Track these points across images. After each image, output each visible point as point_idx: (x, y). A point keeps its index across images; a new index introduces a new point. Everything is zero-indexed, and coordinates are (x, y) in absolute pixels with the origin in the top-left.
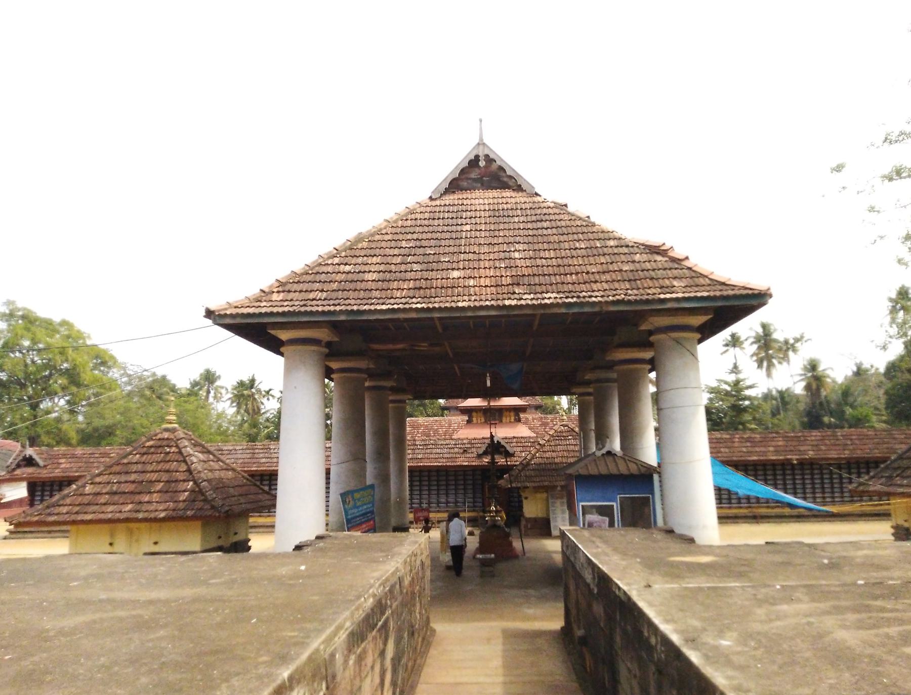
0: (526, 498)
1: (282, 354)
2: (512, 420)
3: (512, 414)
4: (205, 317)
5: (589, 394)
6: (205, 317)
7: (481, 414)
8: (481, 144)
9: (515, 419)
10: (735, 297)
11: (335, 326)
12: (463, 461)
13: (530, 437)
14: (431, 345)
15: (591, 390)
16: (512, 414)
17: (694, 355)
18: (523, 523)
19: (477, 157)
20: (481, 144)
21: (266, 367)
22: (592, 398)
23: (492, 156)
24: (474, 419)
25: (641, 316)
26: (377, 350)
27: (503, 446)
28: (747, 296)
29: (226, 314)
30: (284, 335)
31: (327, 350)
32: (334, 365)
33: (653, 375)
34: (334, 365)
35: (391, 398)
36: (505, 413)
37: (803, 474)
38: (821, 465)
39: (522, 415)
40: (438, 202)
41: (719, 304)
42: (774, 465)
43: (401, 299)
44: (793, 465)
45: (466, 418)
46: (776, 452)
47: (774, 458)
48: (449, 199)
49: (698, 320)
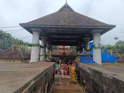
1: (32, 34)
8: (66, 3)
20: (66, 3)
25: (91, 29)
49: (101, 31)
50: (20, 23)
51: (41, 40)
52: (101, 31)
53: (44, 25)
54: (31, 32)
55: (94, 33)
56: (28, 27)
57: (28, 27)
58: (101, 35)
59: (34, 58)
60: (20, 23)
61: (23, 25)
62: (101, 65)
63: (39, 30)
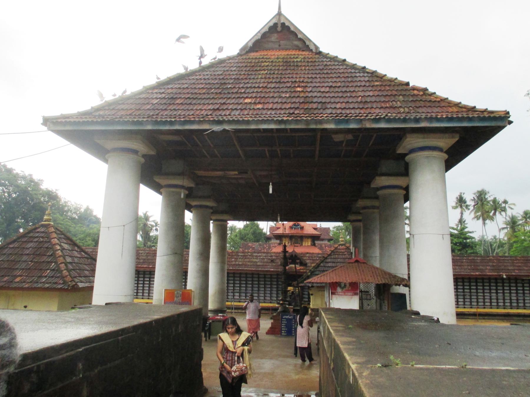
0: (312, 295)
4: (42, 124)
5: (359, 221)
6: (42, 124)
7: (287, 239)
8: (279, 14)
9: (312, 245)
12: (270, 268)
13: (318, 254)
14: (240, 173)
15: (360, 218)
18: (310, 312)
19: (276, 25)
20: (279, 14)
23: (287, 24)
25: (399, 135)
26: (201, 177)
28: (490, 119)
29: (57, 122)
33: (407, 204)
36: (304, 239)
37: (510, 286)
38: (523, 280)
39: (316, 242)
40: (244, 57)
42: (490, 279)
44: (503, 279)
45: (278, 241)
46: (493, 270)
47: (490, 274)
48: (253, 55)
56: (84, 131)
57: (84, 131)
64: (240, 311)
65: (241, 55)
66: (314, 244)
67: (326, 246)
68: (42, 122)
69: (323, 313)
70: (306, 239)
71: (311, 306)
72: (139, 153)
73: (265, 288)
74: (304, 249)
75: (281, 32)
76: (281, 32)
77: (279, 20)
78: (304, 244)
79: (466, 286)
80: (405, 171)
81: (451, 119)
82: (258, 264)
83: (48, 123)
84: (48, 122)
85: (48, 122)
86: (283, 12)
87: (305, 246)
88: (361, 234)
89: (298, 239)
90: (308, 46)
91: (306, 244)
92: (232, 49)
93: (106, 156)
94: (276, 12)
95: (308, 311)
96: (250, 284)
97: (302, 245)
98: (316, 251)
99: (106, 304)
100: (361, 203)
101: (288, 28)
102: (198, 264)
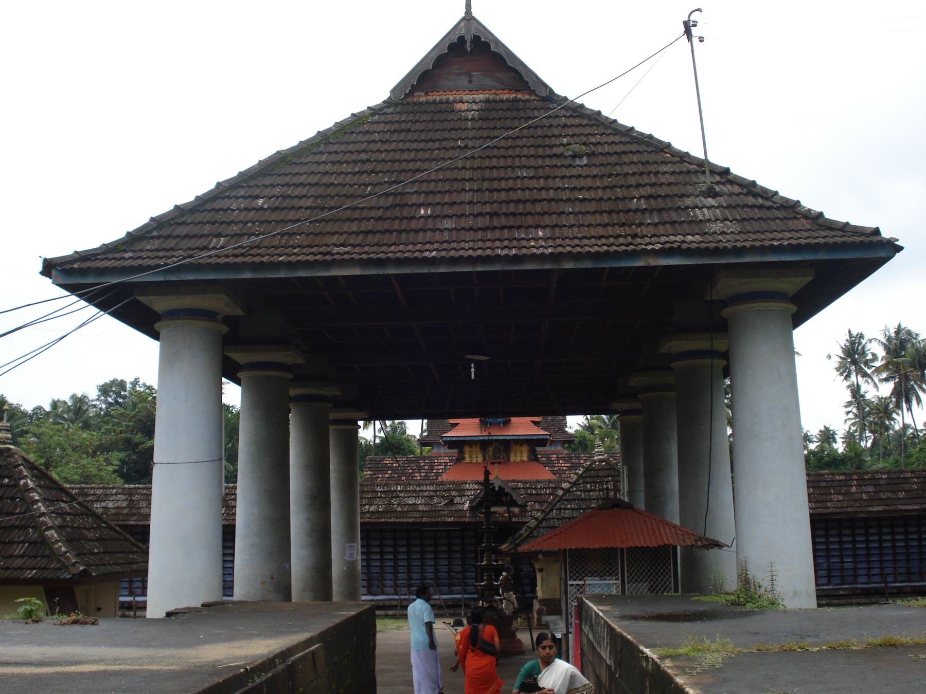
1: (155, 335)
2: (525, 459)
3: (525, 448)
7: (476, 449)
8: (468, 18)
9: (530, 459)
10: (844, 246)
11: (232, 288)
13: (549, 481)
15: (638, 405)
16: (525, 448)
17: (790, 352)
18: (536, 606)
19: (461, 39)
20: (468, 18)
21: (128, 355)
22: (640, 417)
24: (467, 456)
25: (709, 274)
27: (507, 494)
30: (160, 304)
31: (225, 329)
32: (241, 357)
34: (241, 357)
35: (332, 416)
36: (514, 447)
41: (823, 256)
43: (346, 255)
49: (791, 284)
50: (46, 260)
51: (238, 382)
52: (791, 284)
53: (255, 267)
54: (143, 320)
55: (725, 303)
56: (105, 280)
57: (105, 280)
58: (799, 319)
59: (175, 570)
60: (46, 260)
61: (83, 272)
62: (380, 617)
63: (217, 302)
64: (391, 612)
65: (396, 105)
66: (534, 458)
67: (558, 459)
68: (40, 269)
69: (590, 604)
70: (518, 447)
71: (540, 594)
72: (219, 318)
73: (436, 559)
74: (516, 473)
75: (470, 52)
76: (470, 52)
77: (468, 29)
78: (512, 459)
79: (846, 535)
80: (722, 327)
81: (797, 249)
82: (421, 508)
83: (54, 272)
84: (50, 268)
85: (50, 268)
86: (476, 13)
87: (515, 462)
88: (640, 441)
89: (500, 450)
90: (527, 83)
91: (518, 459)
92: (378, 94)
93: (157, 326)
94: (461, 14)
95: (531, 606)
96: (377, 553)
97: (509, 459)
98: (545, 474)
99: (169, 614)
100: (636, 381)
101: (486, 45)
102: (308, 519)
